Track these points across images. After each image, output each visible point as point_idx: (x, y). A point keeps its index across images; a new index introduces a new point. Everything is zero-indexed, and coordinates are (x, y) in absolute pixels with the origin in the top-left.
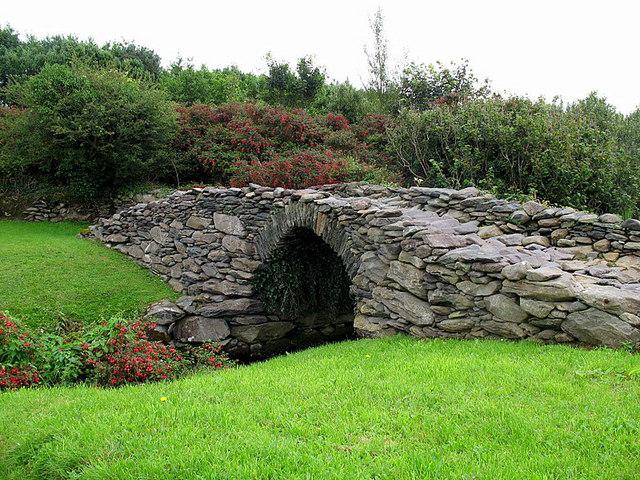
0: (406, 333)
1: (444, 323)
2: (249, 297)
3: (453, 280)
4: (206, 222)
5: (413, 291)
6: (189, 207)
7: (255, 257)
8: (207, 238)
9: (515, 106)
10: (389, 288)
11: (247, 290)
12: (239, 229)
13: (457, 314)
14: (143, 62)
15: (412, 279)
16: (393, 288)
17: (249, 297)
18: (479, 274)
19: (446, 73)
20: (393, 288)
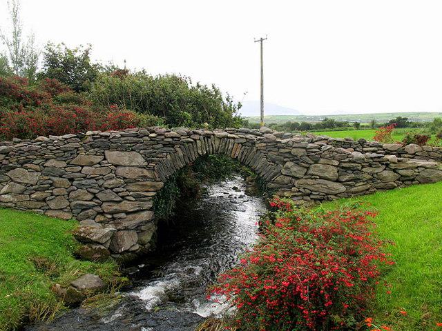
0: (328, 199)
1: (353, 189)
2: (151, 209)
3: (360, 168)
4: (99, 159)
5: (132, 210)
6: (76, 148)
7: (158, 179)
8: (102, 171)
9: (372, 115)
10: (312, 179)
11: (150, 205)
12: (140, 160)
13: (362, 183)
14: (122, 73)
15: (332, 172)
16: (316, 179)
17: (151, 209)
18: (128, 198)
19: (167, 75)
20: (316, 179)
